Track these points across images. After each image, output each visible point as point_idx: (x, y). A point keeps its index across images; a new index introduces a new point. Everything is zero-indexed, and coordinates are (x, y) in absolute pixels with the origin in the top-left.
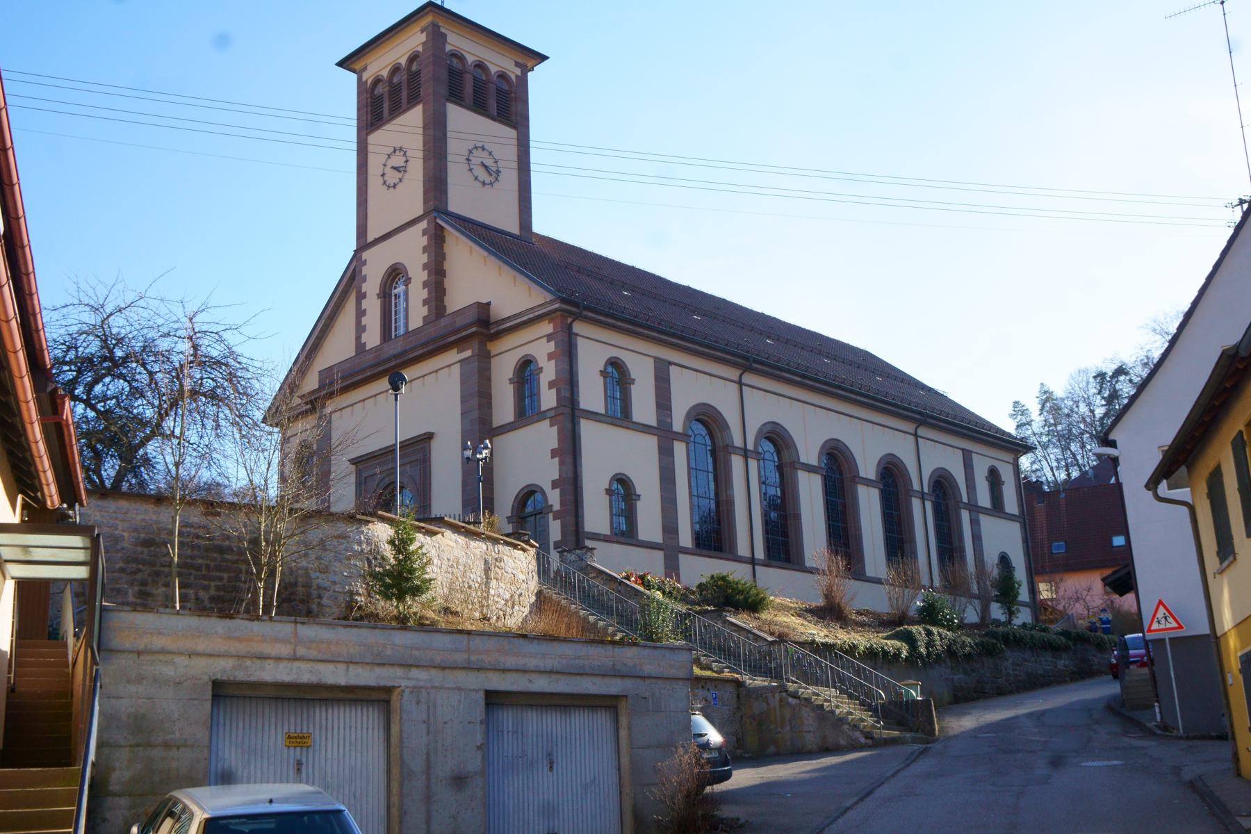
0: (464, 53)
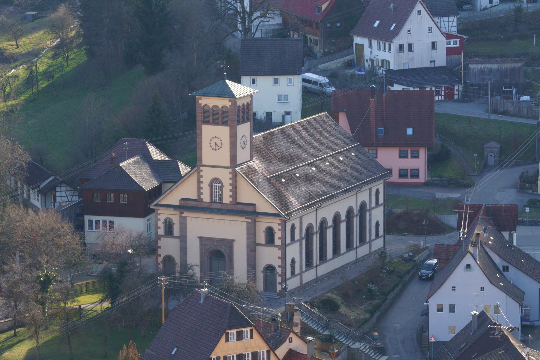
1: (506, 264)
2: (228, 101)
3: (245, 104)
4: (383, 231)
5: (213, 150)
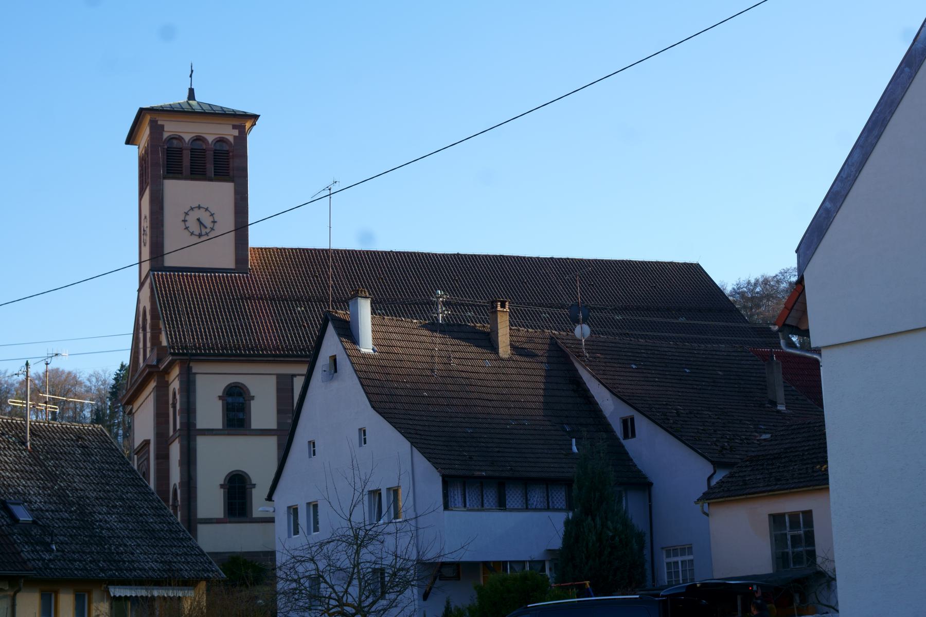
0: (182, 135)
1: (628, 412)
2: (231, 127)
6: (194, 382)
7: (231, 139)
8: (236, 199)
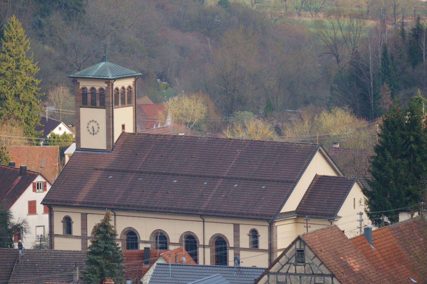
2: (104, 82)
3: (126, 87)
4: (49, 227)
5: (91, 134)
6: (53, 214)
7: (105, 88)
8: (106, 117)
